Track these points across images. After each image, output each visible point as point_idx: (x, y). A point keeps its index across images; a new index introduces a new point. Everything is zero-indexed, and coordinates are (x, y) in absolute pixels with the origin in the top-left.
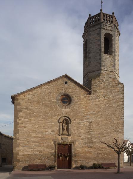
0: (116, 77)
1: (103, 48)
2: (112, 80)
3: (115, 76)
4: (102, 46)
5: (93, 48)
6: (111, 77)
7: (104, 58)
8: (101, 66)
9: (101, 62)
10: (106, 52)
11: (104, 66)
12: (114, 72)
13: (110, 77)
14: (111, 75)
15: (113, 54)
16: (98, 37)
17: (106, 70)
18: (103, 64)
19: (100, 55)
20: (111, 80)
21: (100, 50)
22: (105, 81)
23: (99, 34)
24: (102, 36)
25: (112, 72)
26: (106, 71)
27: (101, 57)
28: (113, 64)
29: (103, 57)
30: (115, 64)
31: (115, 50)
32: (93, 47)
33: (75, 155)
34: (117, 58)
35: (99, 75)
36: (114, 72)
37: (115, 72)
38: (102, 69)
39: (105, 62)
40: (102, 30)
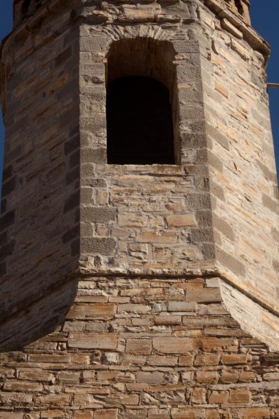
0: (228, 316)
1: (94, 128)
2: (189, 345)
3: (212, 309)
4: (85, 115)
5: (30, 152)
6: (176, 317)
7: (109, 189)
8: (76, 251)
9: (78, 219)
10: (118, 153)
11: (106, 245)
12: (207, 275)
13: (165, 317)
14: (174, 305)
15: (189, 154)
16: (62, 73)
17: (120, 270)
18: (94, 231)
19: (74, 177)
20: (184, 342)
21: (74, 145)
22: (112, 357)
23: (69, 58)
24: (85, 59)
25: (190, 277)
26: (120, 282)
27: (78, 185)
28: (191, 219)
29: (100, 183)
30: (206, 218)
31: (200, 126)
32: (27, 149)
33: (265, 109)
34: (264, 111)
35: (61, 315)
36: (207, 275)
37: (215, 275)
38: (90, 267)
39: (108, 214)
40: (84, 29)
